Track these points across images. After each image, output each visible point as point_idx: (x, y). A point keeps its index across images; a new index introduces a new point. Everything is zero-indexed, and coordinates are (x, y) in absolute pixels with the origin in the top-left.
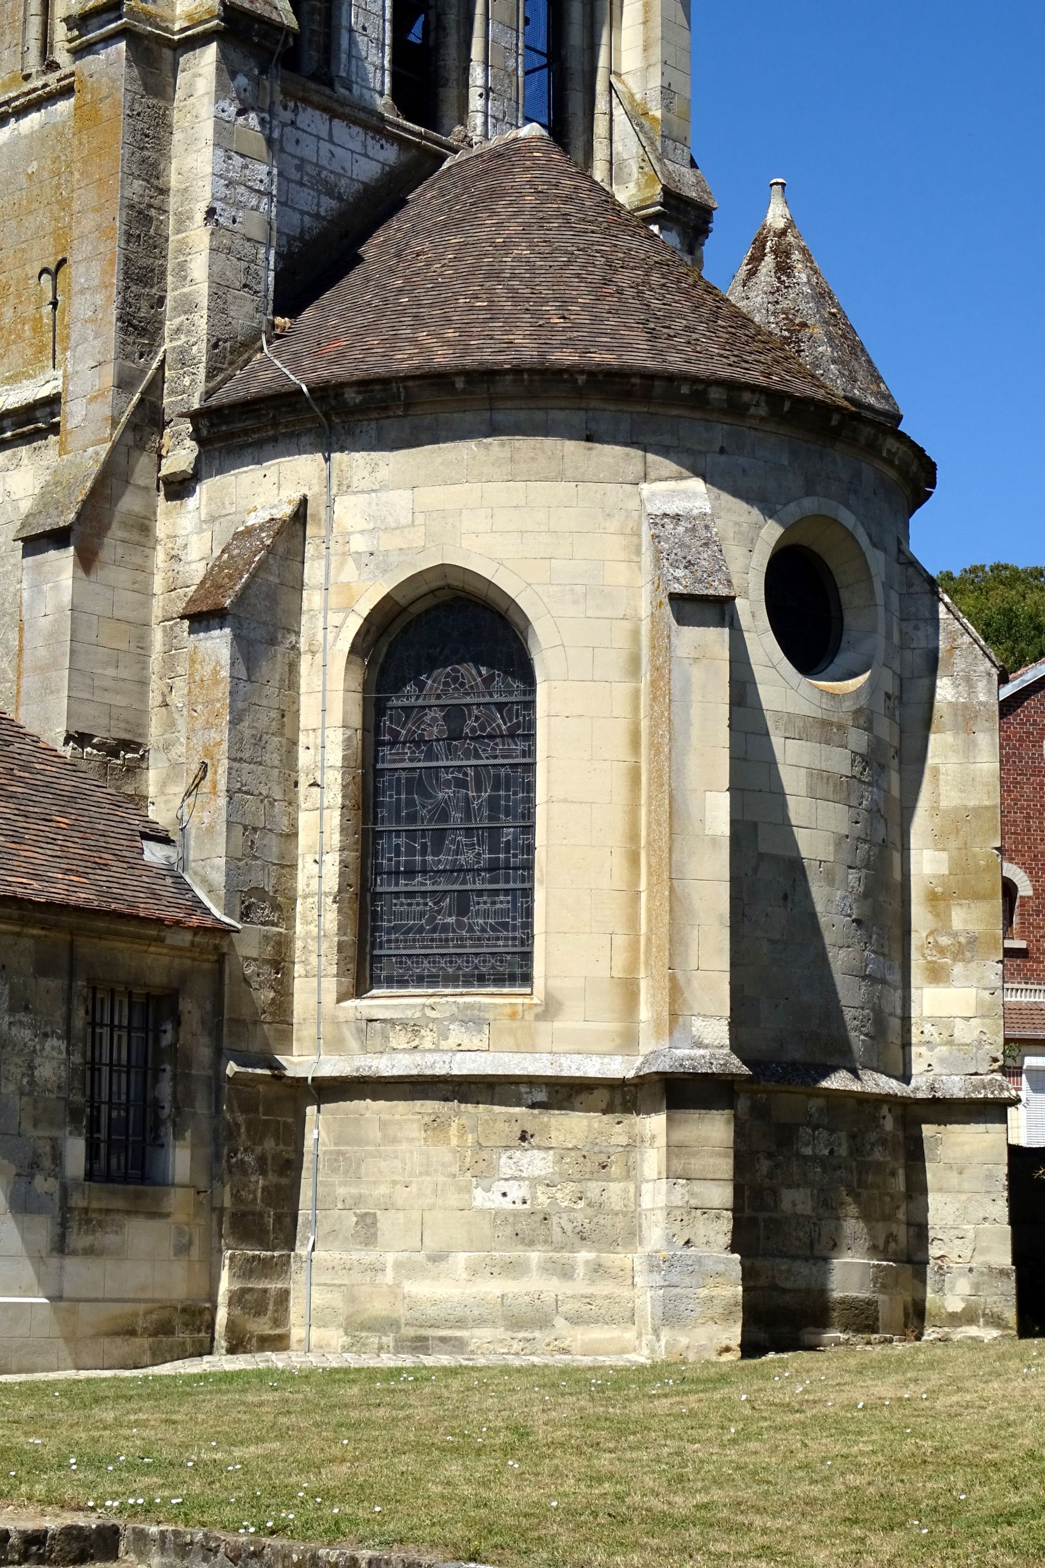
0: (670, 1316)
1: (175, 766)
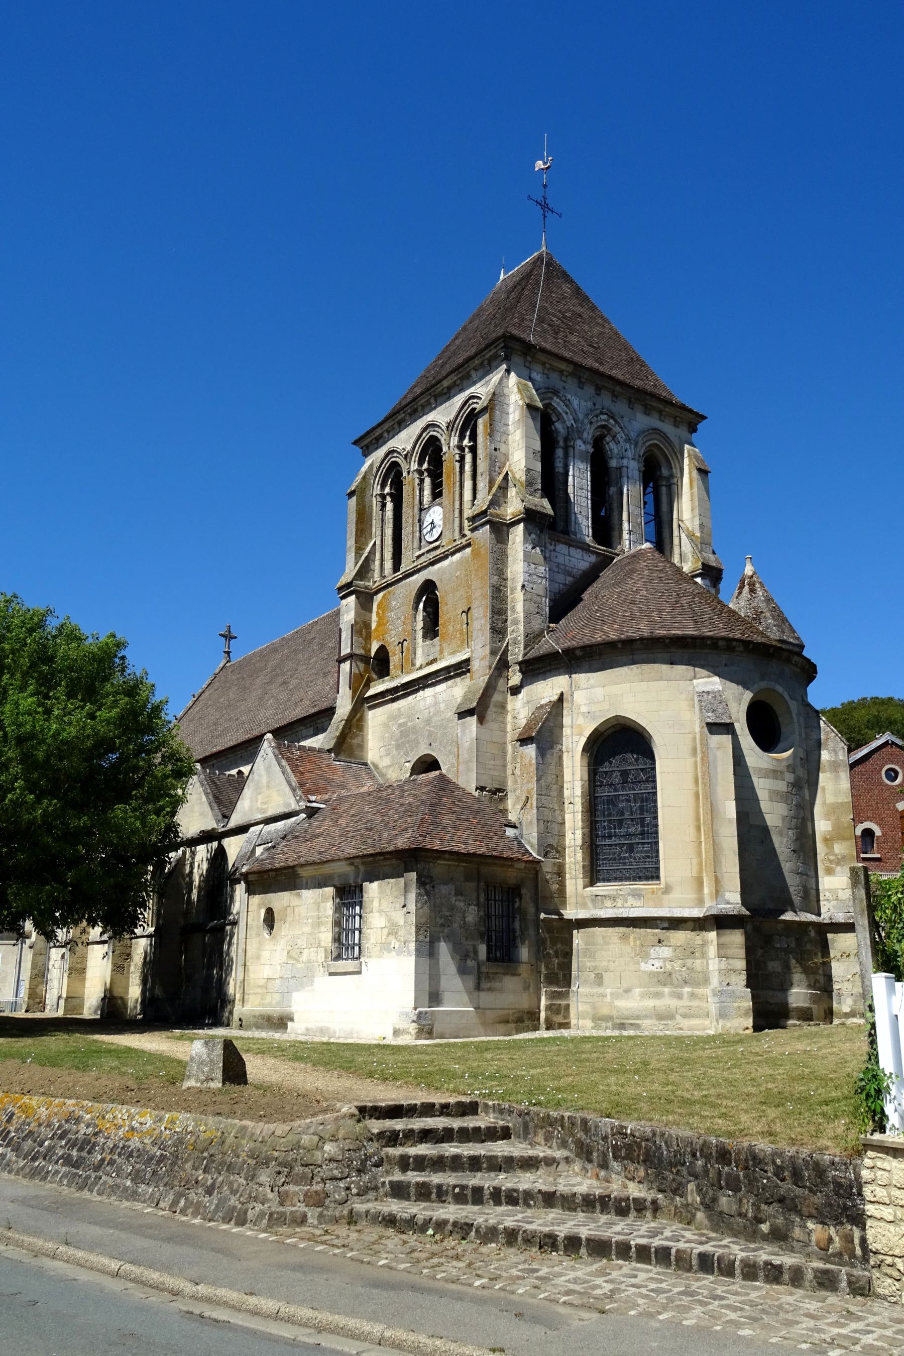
0: (723, 1015)
1: (518, 798)
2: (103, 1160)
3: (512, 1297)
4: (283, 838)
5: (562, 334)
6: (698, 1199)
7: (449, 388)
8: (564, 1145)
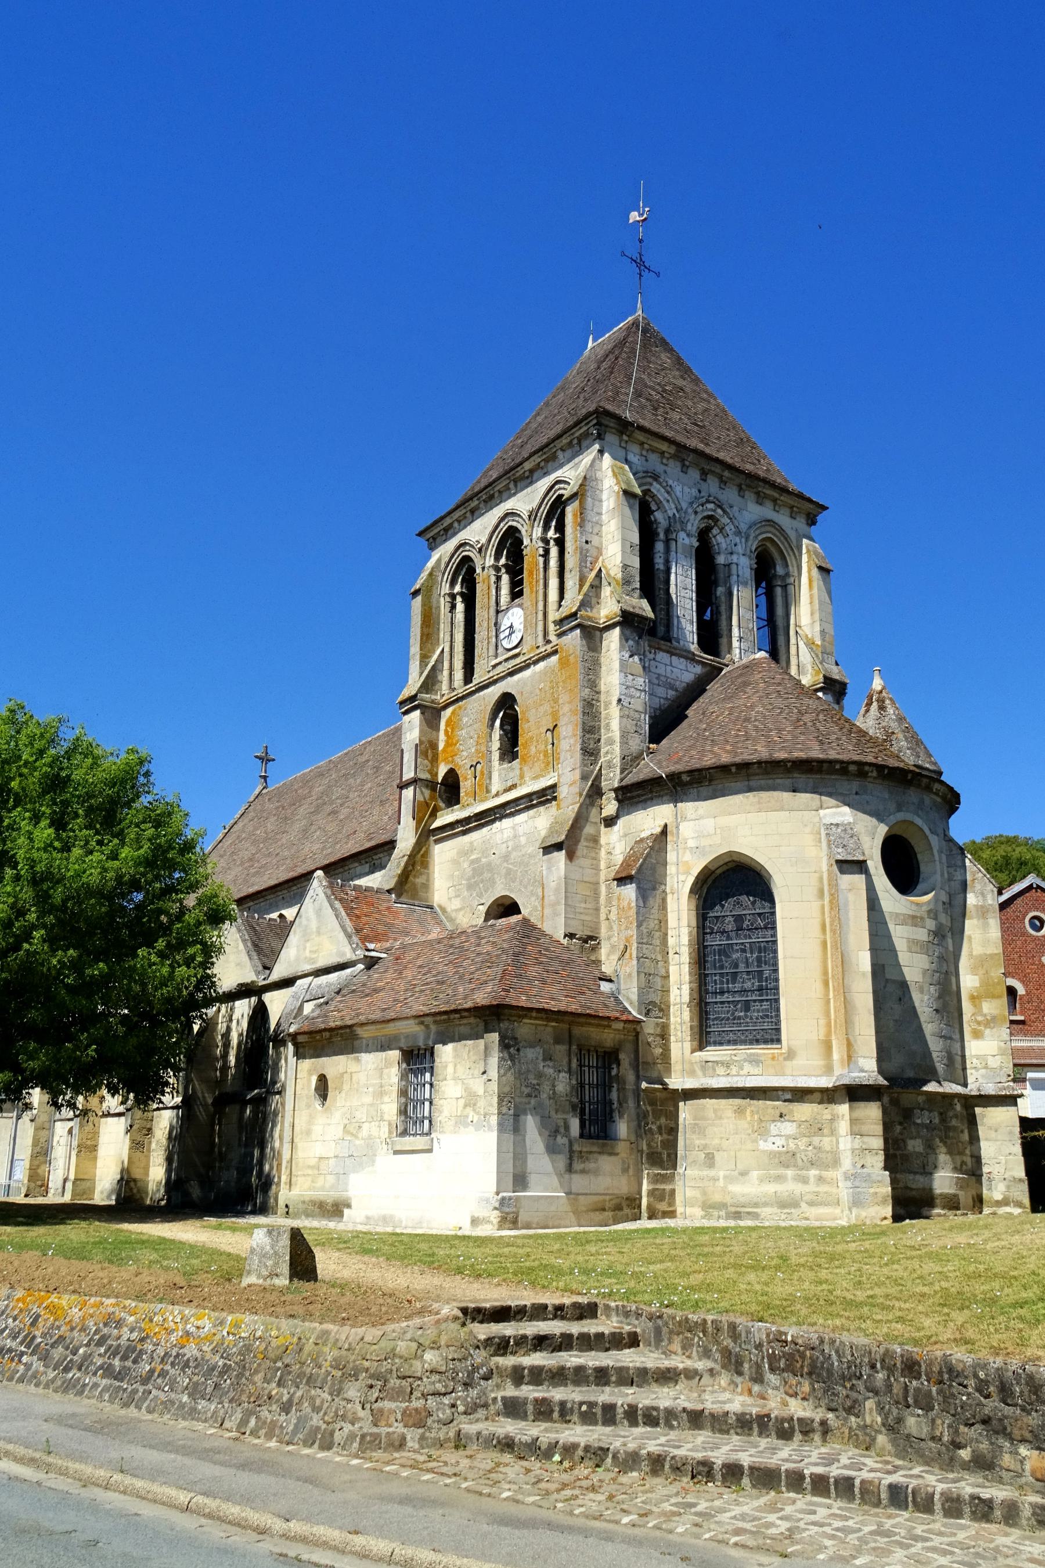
0: (857, 1202)
1: (613, 947)
2: (152, 1371)
3: (670, 1536)
4: (338, 993)
5: (661, 410)
6: (879, 1419)
7: (532, 471)
8: (706, 1354)
